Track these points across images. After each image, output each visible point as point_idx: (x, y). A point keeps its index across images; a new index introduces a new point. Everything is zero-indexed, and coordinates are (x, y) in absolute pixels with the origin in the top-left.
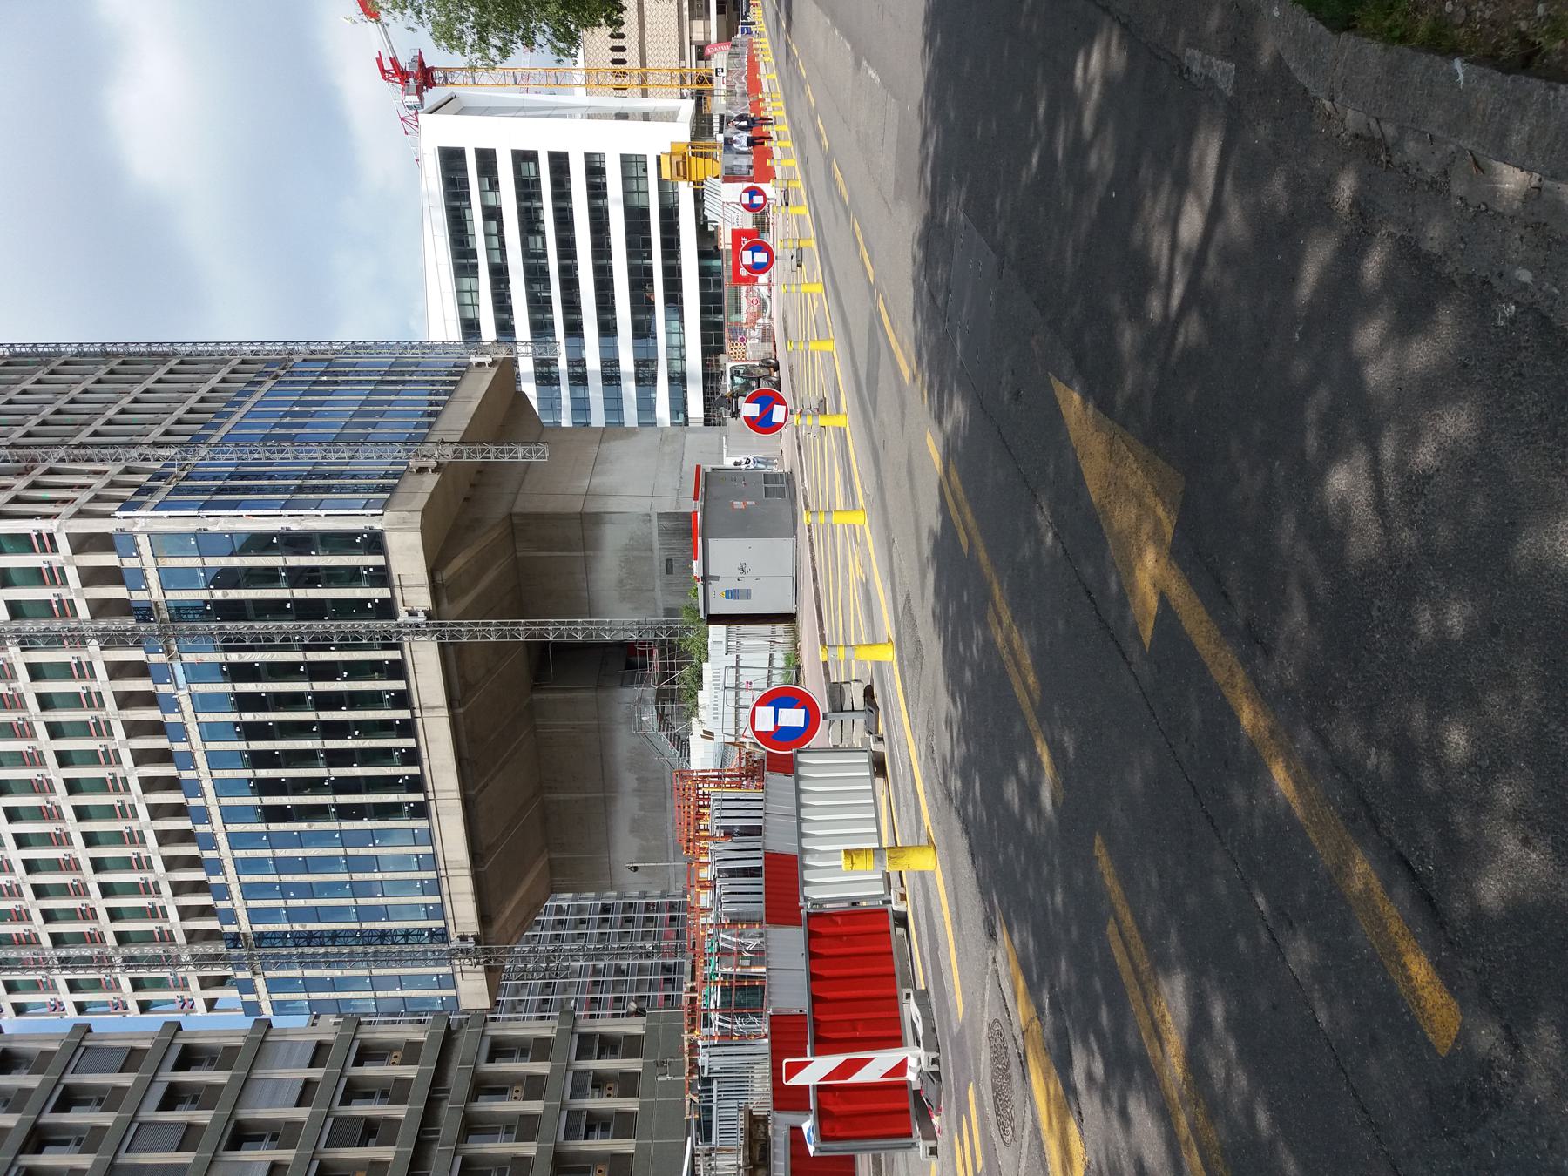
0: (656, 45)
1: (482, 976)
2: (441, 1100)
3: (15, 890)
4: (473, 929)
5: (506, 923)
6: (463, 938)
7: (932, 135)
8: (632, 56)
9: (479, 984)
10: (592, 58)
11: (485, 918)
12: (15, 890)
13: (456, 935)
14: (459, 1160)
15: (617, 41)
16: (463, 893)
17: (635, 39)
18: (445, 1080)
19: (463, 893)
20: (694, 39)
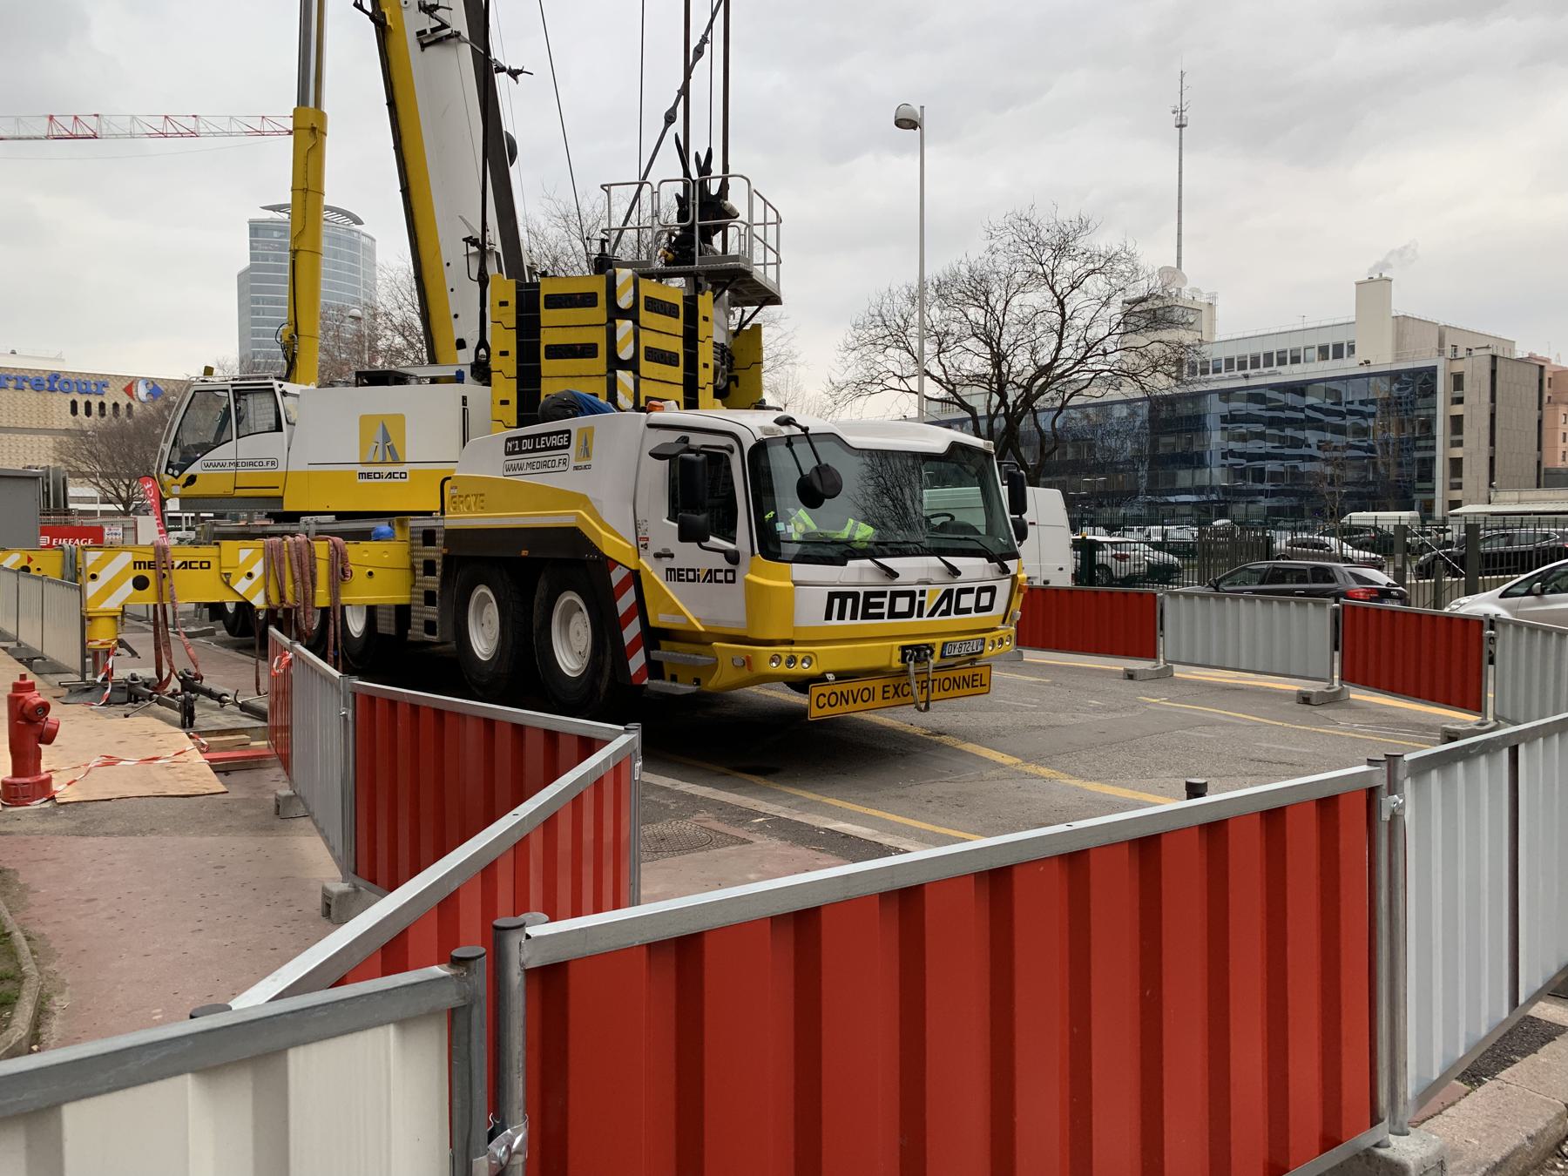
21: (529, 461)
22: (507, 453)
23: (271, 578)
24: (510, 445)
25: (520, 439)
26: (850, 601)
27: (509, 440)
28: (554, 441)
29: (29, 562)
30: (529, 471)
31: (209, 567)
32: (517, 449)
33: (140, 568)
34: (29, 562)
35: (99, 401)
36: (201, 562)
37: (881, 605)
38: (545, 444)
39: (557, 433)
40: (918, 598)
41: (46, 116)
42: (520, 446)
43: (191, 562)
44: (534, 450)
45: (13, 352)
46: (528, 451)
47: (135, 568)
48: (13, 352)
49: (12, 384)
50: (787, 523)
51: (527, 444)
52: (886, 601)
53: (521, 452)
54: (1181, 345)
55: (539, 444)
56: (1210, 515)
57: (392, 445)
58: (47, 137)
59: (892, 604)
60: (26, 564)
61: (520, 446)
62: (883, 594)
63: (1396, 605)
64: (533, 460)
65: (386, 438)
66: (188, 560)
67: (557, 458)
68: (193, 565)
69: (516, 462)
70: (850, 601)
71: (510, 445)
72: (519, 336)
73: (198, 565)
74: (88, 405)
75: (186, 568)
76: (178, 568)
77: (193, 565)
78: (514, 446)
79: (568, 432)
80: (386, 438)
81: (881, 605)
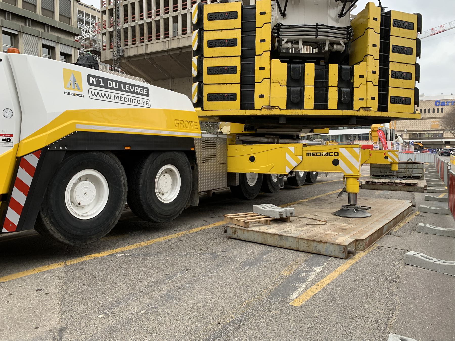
0: (401, 123)
1: (111, 58)
2: (44, 29)
3: (185, 32)
4: (126, 55)
5: (129, 66)
6: (123, 51)
7: (209, 132)
8: (427, 115)
9: (109, 57)
10: (426, 103)
11: (129, 58)
12: (185, 32)
13: (124, 49)
14: (16, 33)
15: (436, 111)
16: (137, 51)
17: (424, 117)
18: (51, 32)
19: (137, 51)
20: (403, 135)
26: (310, 154)
31: (338, 155)
33: (309, 156)
35: (441, 108)
36: (335, 153)
37: (315, 154)
40: (321, 154)
41: (431, 29)
43: (330, 153)
44: (130, 92)
45: (452, 94)
47: (307, 156)
48: (452, 94)
49: (450, 104)
52: (316, 154)
57: (77, 83)
58: (431, 35)
59: (317, 154)
62: (315, 153)
65: (75, 80)
66: (329, 152)
68: (331, 154)
70: (310, 154)
72: (327, 83)
73: (333, 154)
74: (438, 109)
75: (328, 156)
76: (325, 156)
77: (331, 154)
80: (75, 80)
81: (315, 154)
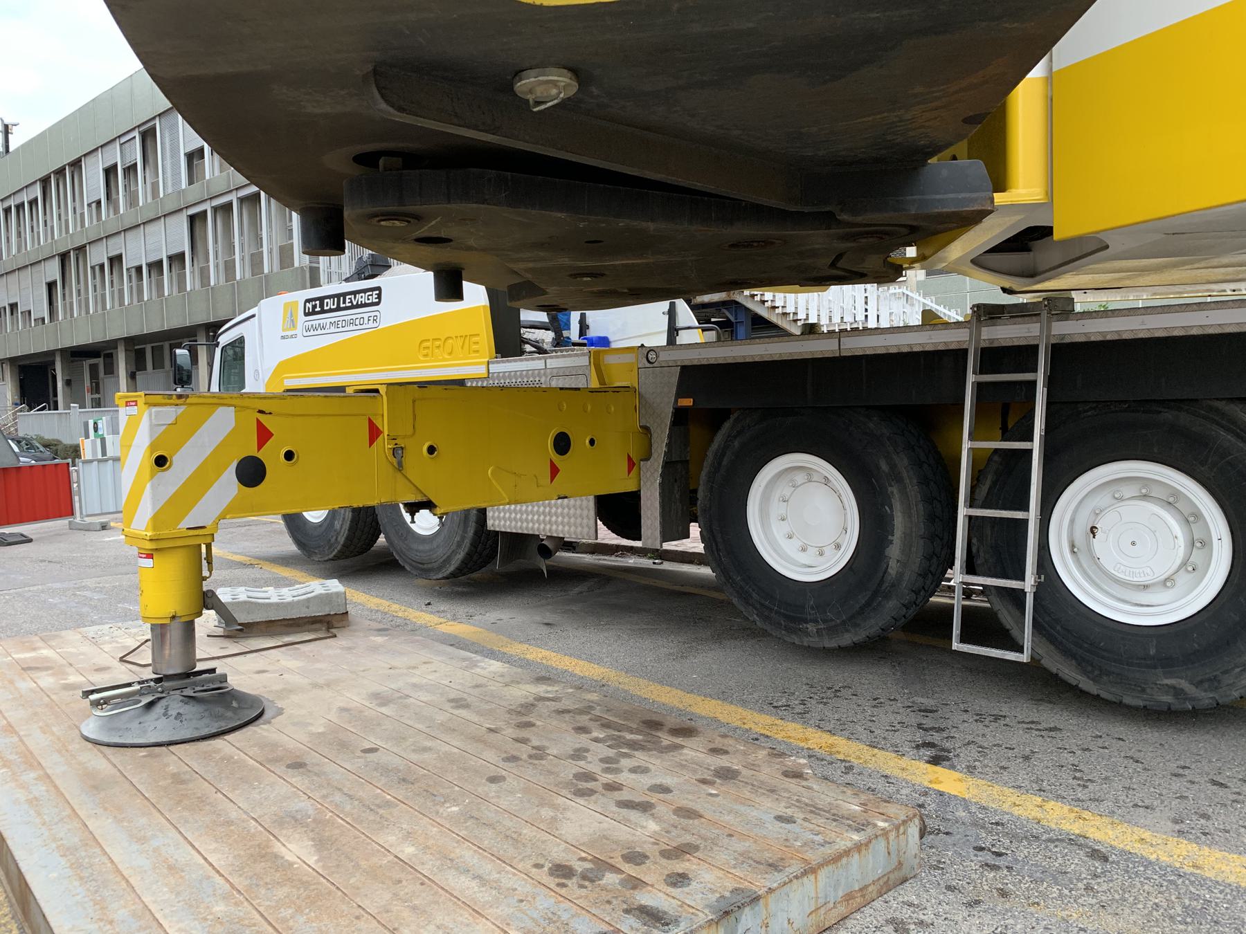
21: (332, 320)
22: (306, 314)
23: (843, 273)
24: (309, 305)
25: (321, 299)
27: (308, 301)
28: (361, 298)
29: (261, 444)
30: (333, 329)
32: (318, 309)
34: (261, 444)
38: (351, 302)
39: (365, 291)
42: (322, 305)
44: (339, 309)
46: (331, 310)
50: (920, 286)
51: (330, 304)
53: (323, 311)
54: (1056, 639)
55: (344, 302)
56: (261, 278)
60: (252, 451)
61: (322, 305)
63: (657, 561)
64: (336, 319)
67: (366, 316)
69: (317, 322)
71: (309, 305)
78: (314, 307)
79: (379, 289)
